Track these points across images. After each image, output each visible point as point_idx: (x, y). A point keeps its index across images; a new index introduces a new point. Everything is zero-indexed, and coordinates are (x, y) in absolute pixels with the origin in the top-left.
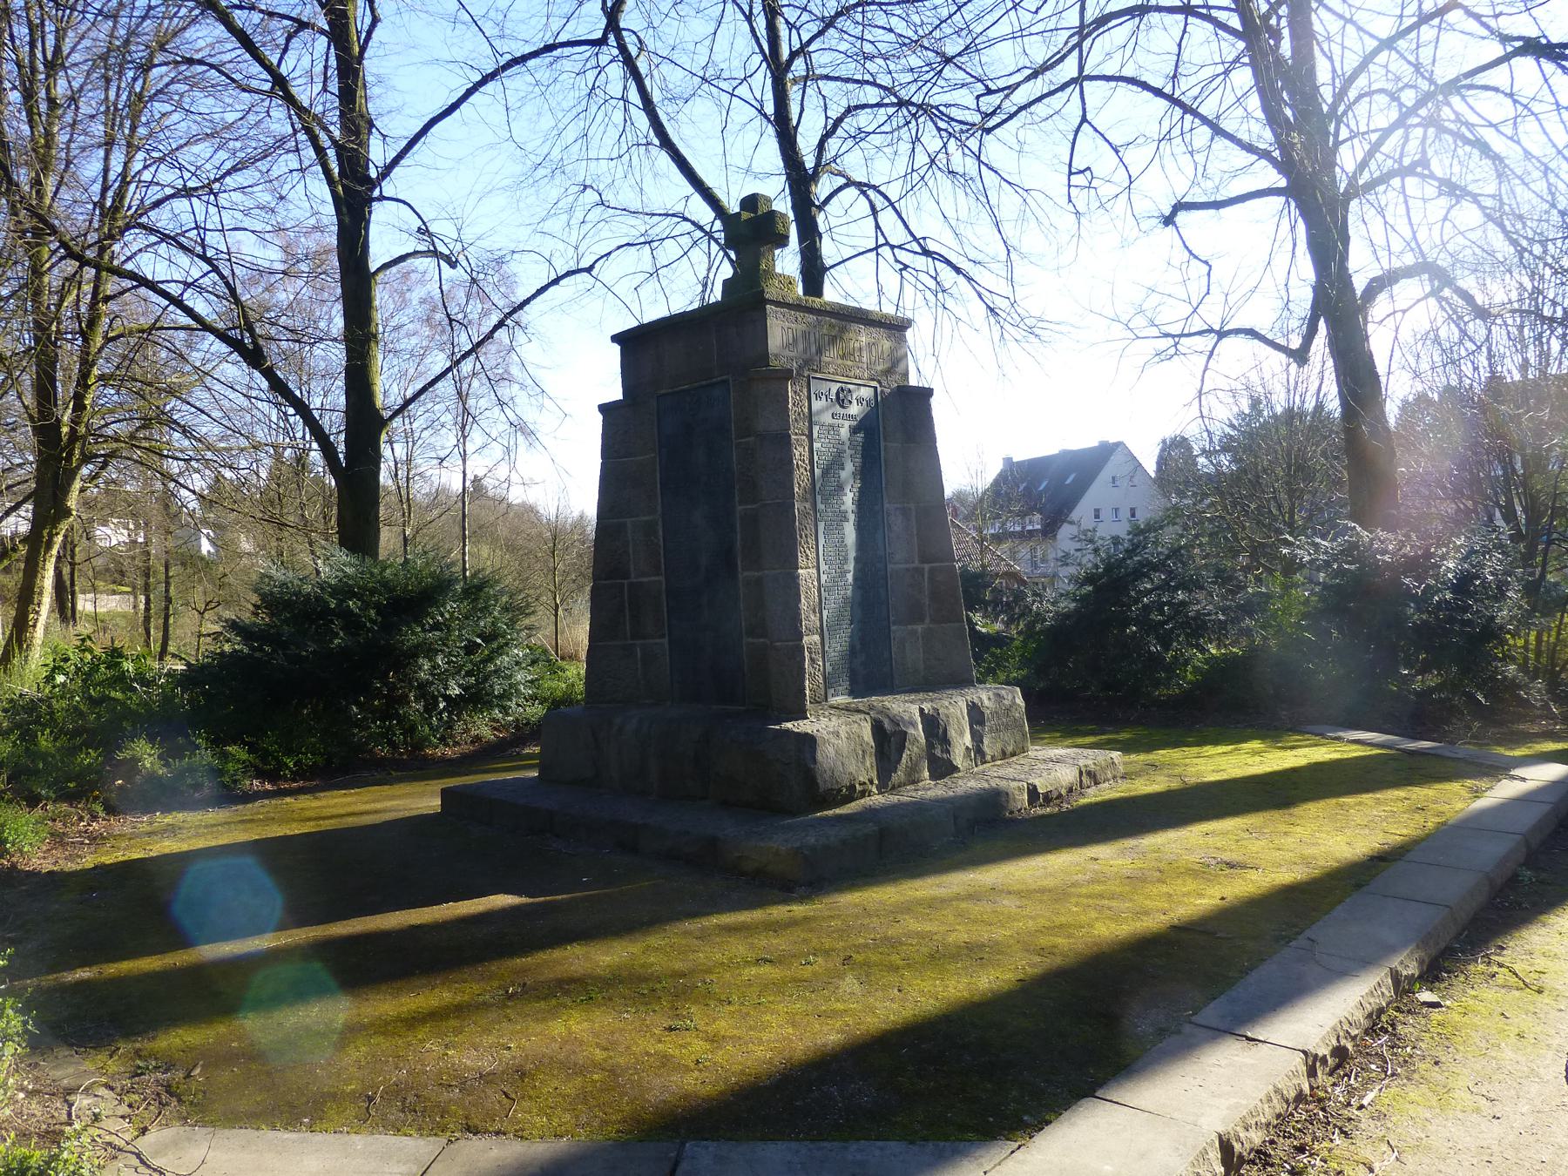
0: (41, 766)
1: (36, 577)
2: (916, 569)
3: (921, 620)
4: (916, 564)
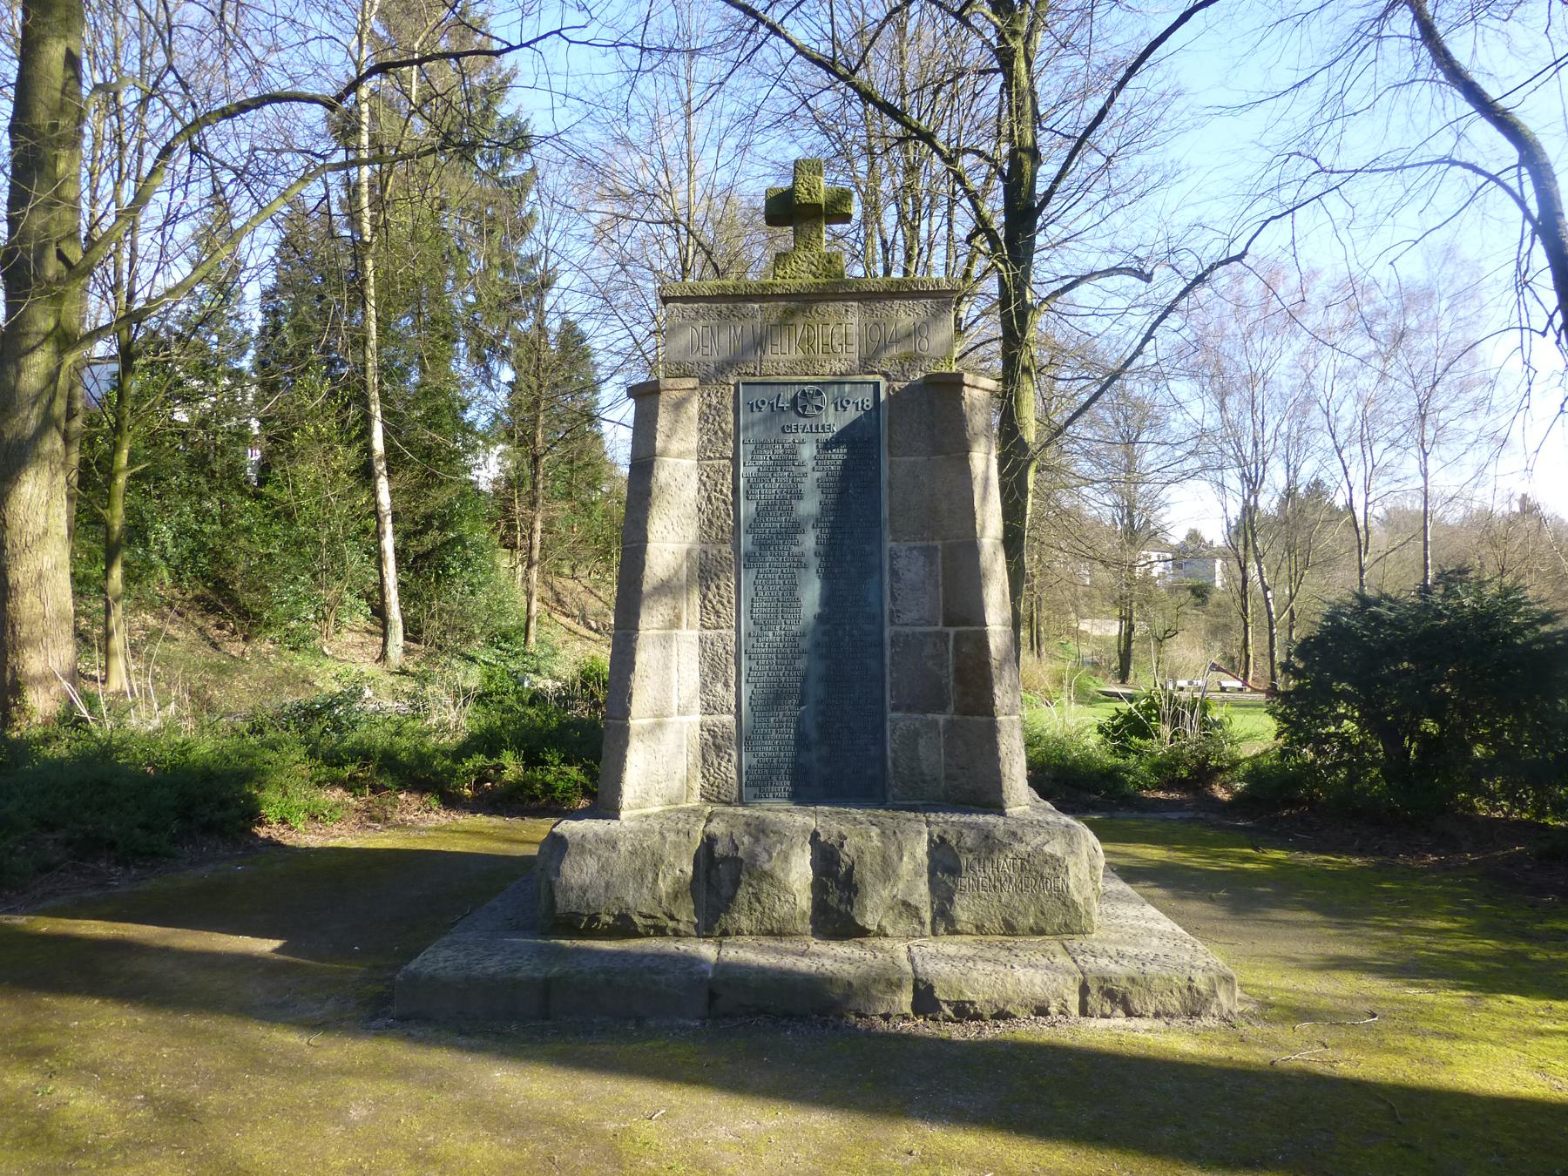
0: (1430, 726)
1: (4, 632)
2: (938, 634)
3: (942, 708)
4: (940, 627)
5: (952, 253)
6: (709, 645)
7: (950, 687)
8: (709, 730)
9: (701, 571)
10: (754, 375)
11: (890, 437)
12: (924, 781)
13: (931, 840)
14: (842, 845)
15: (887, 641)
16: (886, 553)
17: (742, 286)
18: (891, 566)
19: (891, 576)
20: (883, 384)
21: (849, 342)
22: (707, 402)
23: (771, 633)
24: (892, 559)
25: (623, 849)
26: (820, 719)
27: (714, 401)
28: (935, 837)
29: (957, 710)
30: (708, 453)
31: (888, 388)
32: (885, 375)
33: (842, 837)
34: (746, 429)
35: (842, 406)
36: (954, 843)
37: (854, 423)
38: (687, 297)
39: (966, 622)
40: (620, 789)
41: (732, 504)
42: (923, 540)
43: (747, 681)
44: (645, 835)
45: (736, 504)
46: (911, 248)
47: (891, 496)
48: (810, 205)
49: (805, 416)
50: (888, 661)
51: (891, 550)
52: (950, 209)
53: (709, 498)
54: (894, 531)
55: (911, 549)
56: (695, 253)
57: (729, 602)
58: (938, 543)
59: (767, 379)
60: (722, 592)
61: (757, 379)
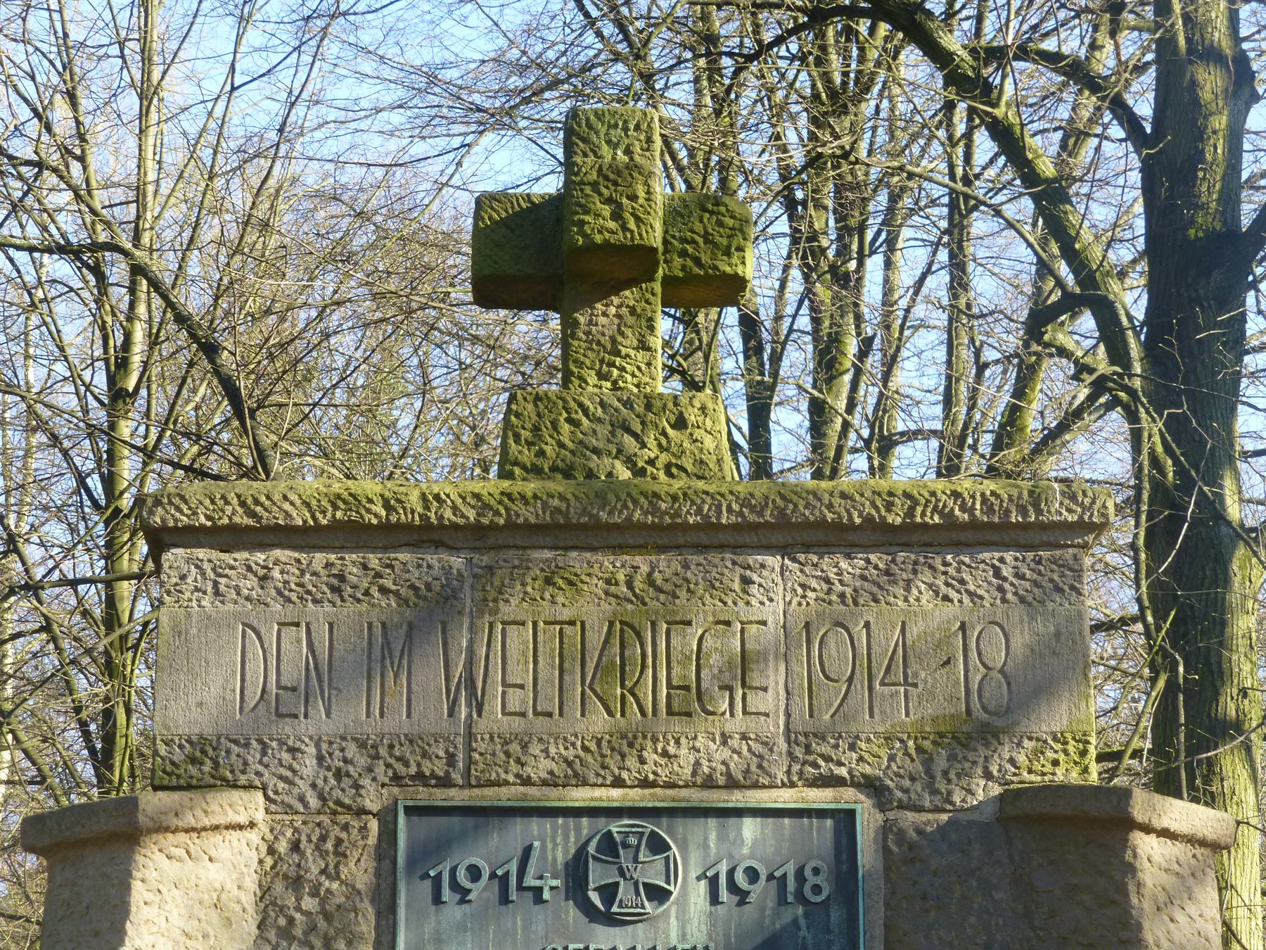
5: (966, 354)
10: (445, 782)
17: (414, 499)
31: (886, 829)
32: (872, 786)
38: (233, 528)
46: (836, 340)
48: (621, 249)
52: (956, 232)
56: (154, 341)
59: (489, 796)
61: (457, 796)
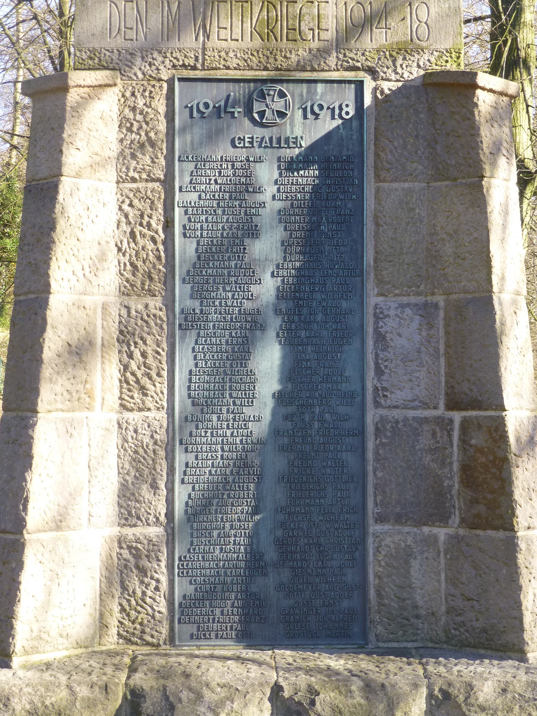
2: (439, 421)
4: (441, 411)
6: (131, 433)
7: (454, 492)
8: (130, 548)
9: (121, 332)
10: (194, 68)
11: (377, 155)
12: (418, 617)
13: (430, 696)
14: (313, 703)
15: (370, 429)
16: (369, 312)
18: (376, 330)
19: (376, 342)
20: (369, 85)
21: (323, 26)
22: (131, 103)
23: (215, 417)
24: (376, 317)
25: (18, 708)
26: (279, 533)
27: (141, 102)
28: (436, 692)
29: (463, 521)
30: (131, 174)
31: (375, 89)
33: (313, 692)
34: (183, 130)
35: (313, 112)
36: (461, 698)
37: (328, 136)
39: (477, 405)
40: (12, 627)
41: (164, 243)
42: (419, 294)
43: (183, 482)
44: (47, 689)
45: (169, 242)
47: (376, 235)
49: (262, 125)
50: (370, 455)
51: (376, 306)
53: (133, 235)
54: (380, 282)
55: (403, 306)
57: (159, 375)
58: (440, 300)
60: (150, 360)
61: (199, 74)
